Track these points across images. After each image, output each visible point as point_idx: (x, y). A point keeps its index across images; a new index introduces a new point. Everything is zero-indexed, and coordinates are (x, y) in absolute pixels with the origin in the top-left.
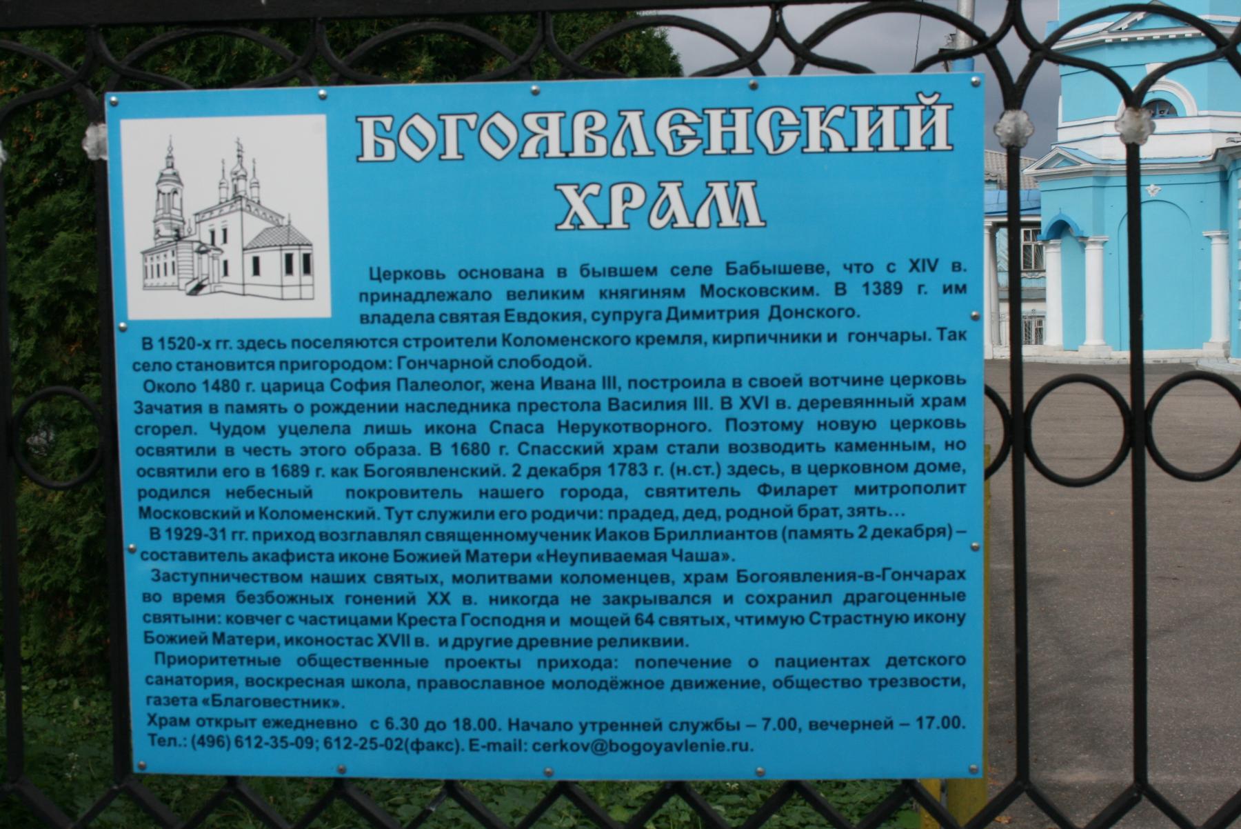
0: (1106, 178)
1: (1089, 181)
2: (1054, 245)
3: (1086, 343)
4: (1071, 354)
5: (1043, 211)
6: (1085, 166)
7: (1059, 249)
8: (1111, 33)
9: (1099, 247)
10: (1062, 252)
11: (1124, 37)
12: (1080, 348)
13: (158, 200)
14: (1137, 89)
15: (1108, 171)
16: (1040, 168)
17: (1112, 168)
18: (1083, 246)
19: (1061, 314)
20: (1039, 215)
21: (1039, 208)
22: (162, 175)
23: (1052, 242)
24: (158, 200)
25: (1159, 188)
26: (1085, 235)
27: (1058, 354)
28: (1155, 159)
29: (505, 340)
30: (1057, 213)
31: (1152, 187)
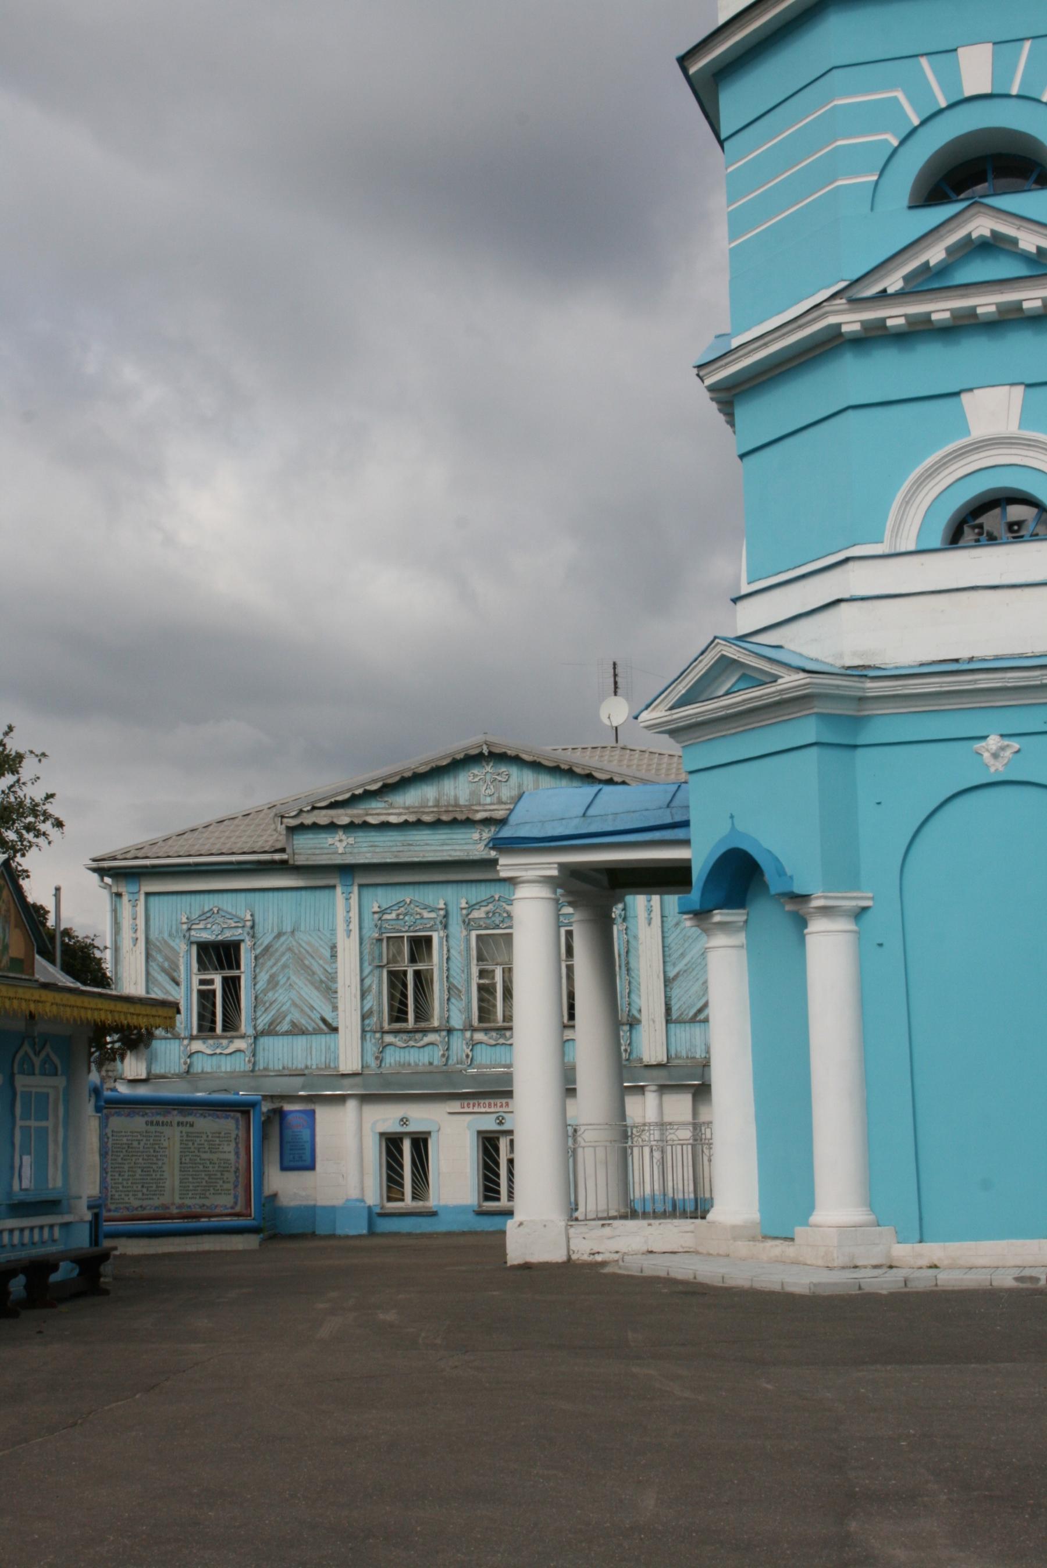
0: (858, 722)
1: (807, 730)
2: (723, 926)
3: (816, 1218)
4: (776, 1249)
5: (694, 832)
6: (789, 680)
7: (741, 938)
8: (856, 303)
9: (844, 924)
10: (752, 950)
11: (895, 316)
12: (799, 1231)
13: (712, 1134)
14: (976, 238)
15: (861, 699)
16: (683, 702)
17: (873, 688)
18: (801, 922)
19: (752, 1130)
20: (686, 843)
21: (685, 824)
22: (461, 1071)
23: (718, 916)
24: (712, 1134)
25: (1015, 744)
26: (798, 890)
27: (743, 1248)
28: (997, 658)
29: (156, 1132)
30: (724, 829)
31: (993, 742)
